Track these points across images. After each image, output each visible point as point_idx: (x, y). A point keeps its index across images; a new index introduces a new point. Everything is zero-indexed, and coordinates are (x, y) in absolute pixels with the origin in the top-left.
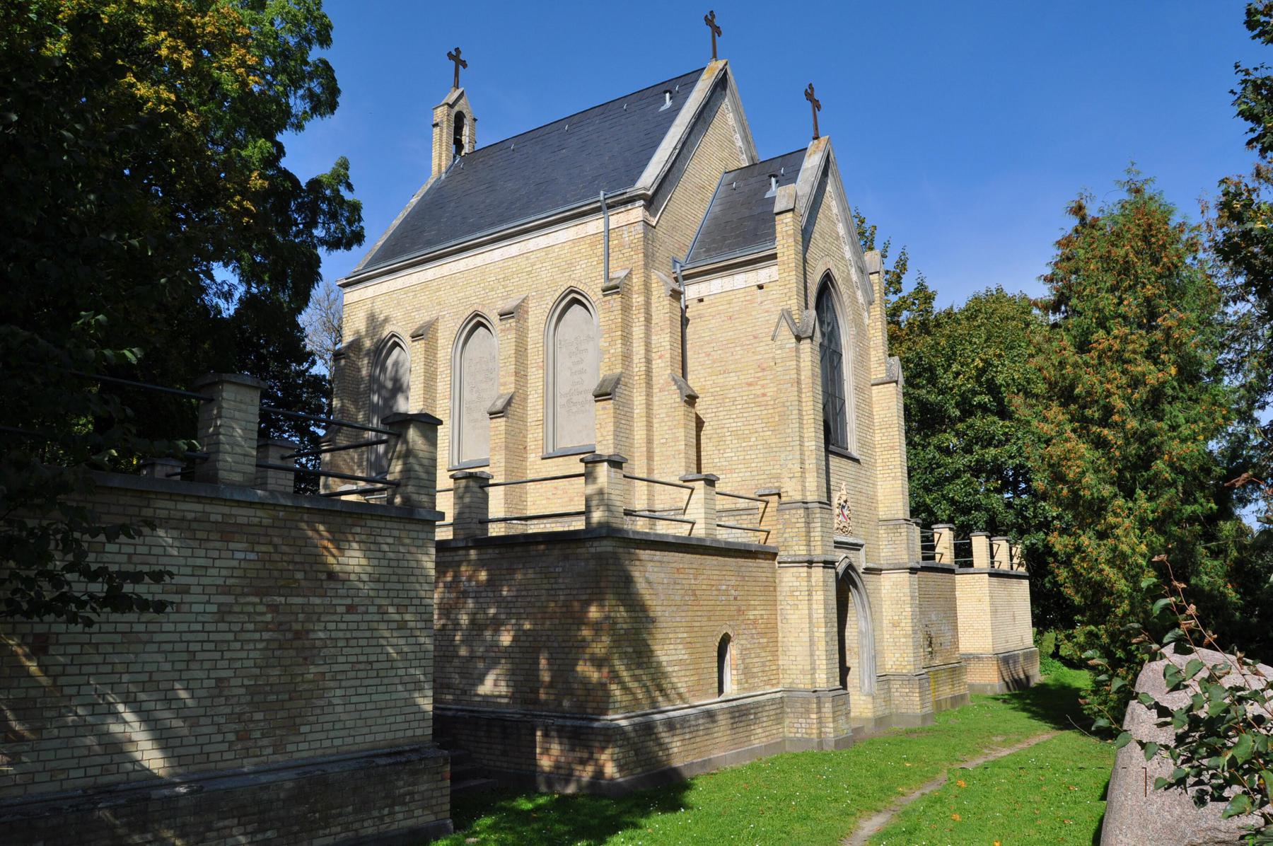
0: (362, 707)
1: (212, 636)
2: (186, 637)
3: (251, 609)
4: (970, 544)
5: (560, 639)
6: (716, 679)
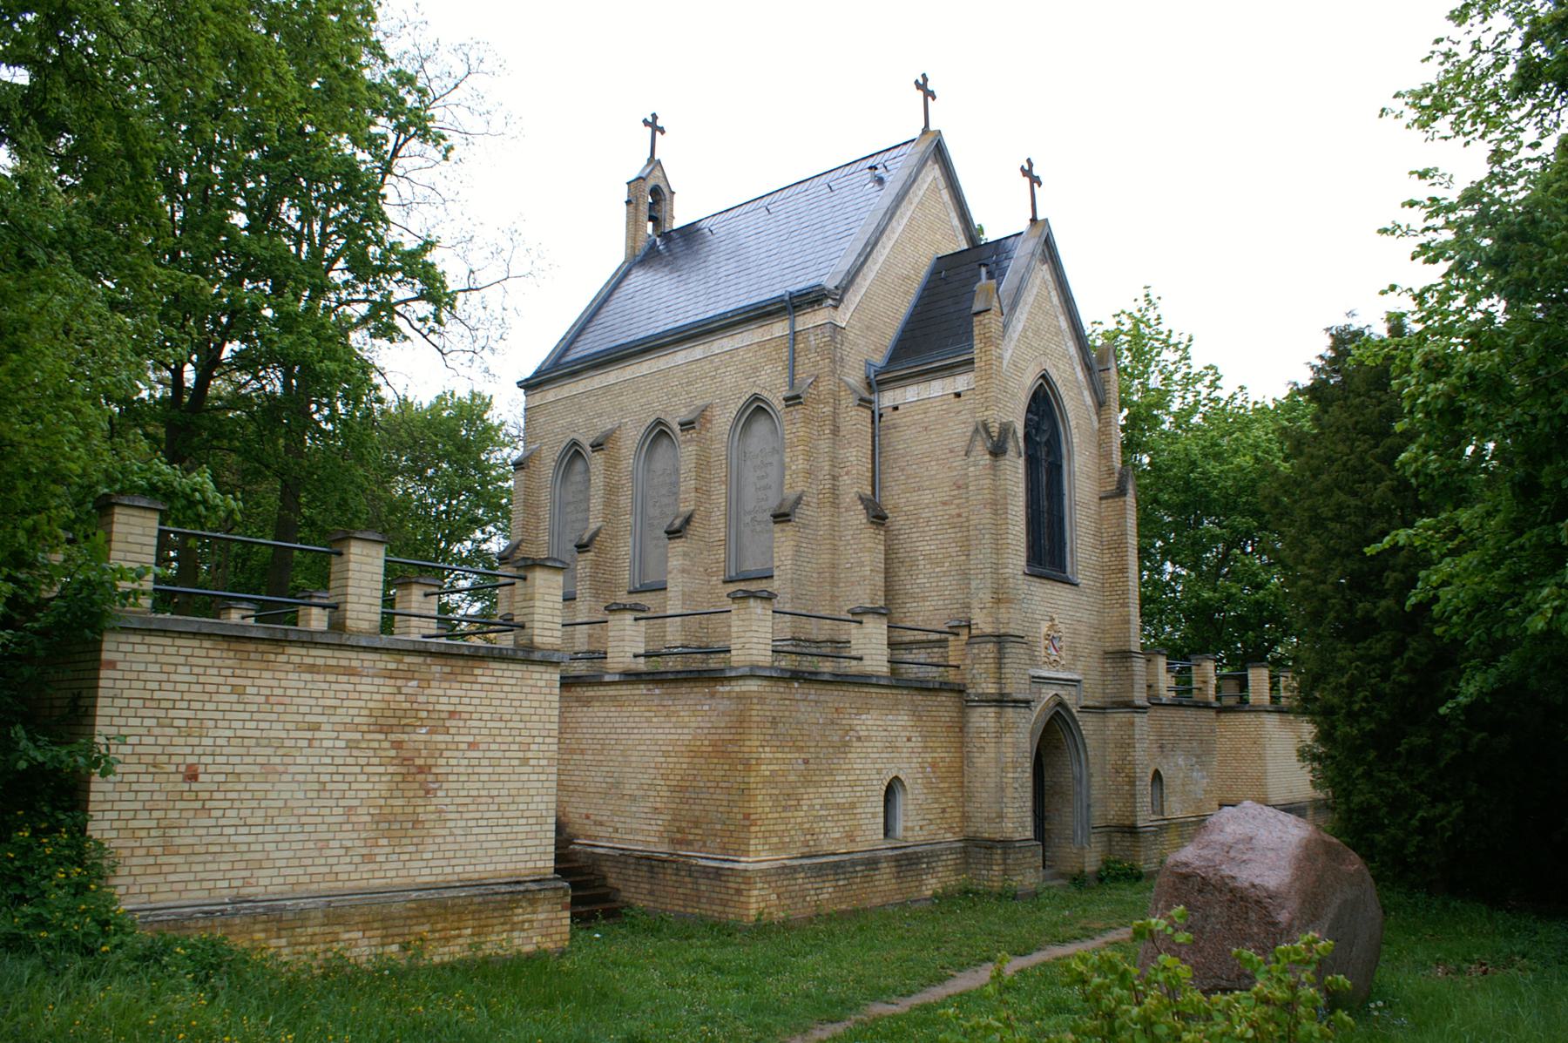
0: (483, 838)
1: (341, 769)
2: (317, 769)
3: (376, 745)
4: (1246, 676)
5: (705, 778)
6: (882, 826)
